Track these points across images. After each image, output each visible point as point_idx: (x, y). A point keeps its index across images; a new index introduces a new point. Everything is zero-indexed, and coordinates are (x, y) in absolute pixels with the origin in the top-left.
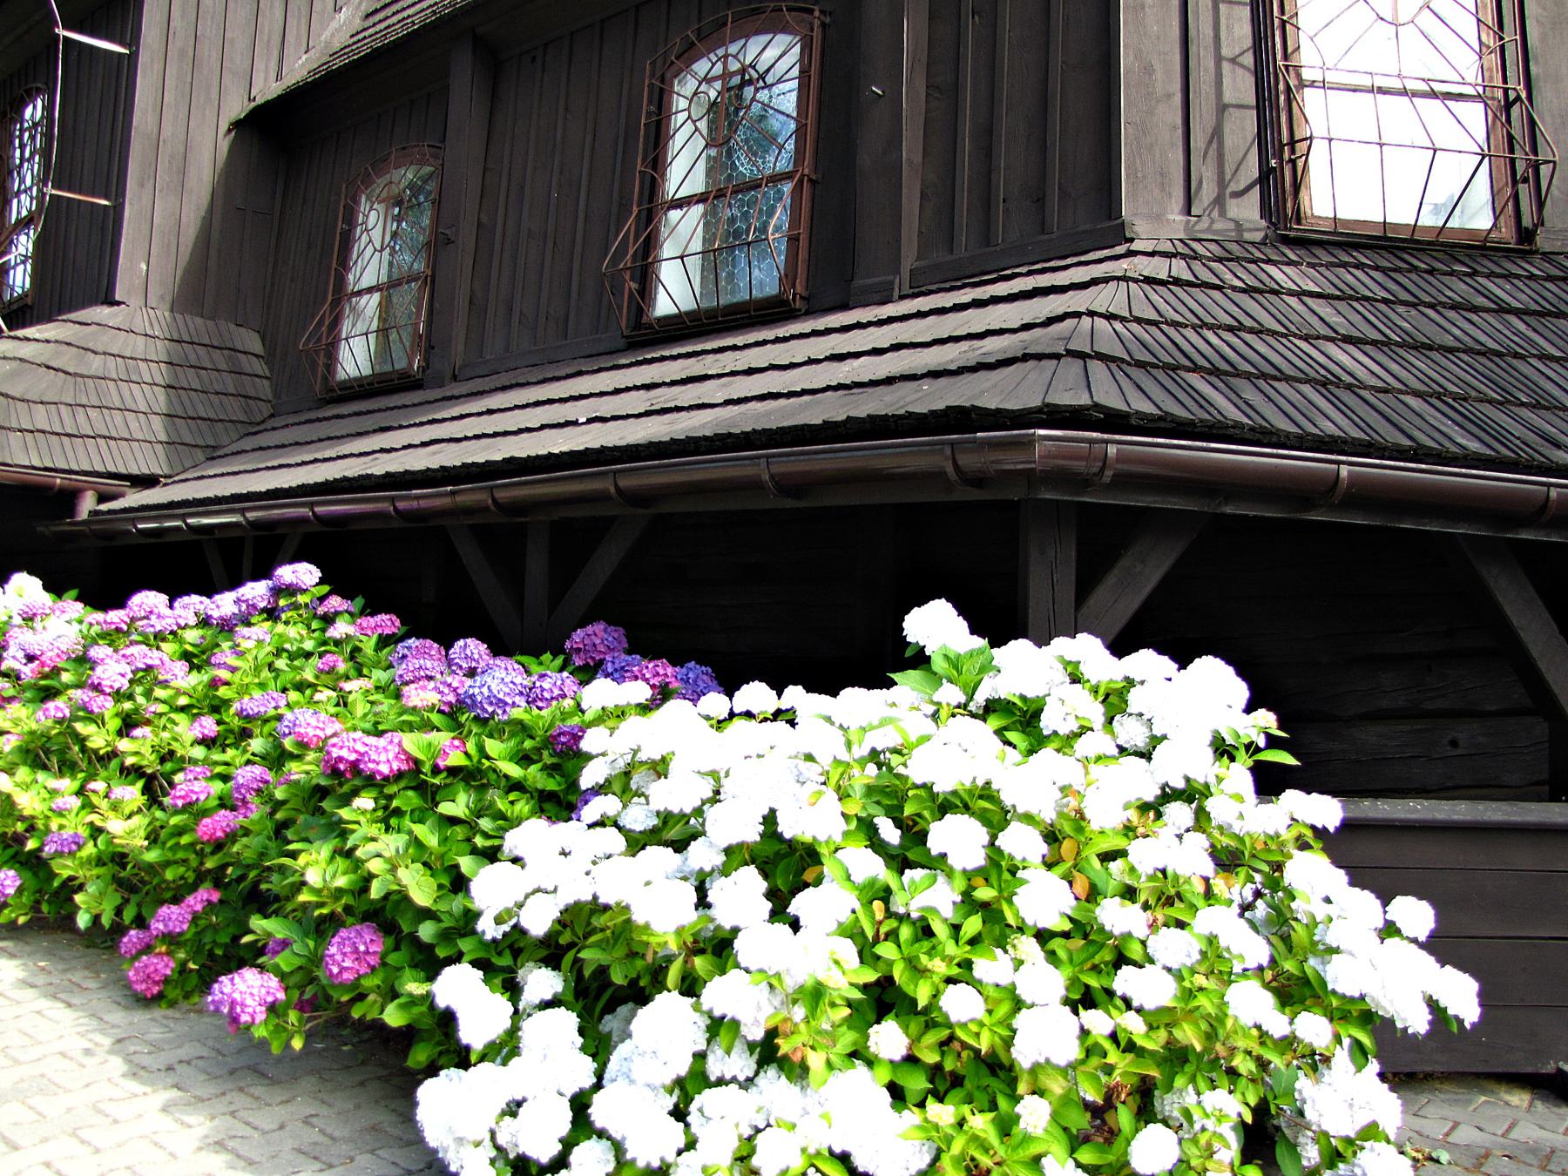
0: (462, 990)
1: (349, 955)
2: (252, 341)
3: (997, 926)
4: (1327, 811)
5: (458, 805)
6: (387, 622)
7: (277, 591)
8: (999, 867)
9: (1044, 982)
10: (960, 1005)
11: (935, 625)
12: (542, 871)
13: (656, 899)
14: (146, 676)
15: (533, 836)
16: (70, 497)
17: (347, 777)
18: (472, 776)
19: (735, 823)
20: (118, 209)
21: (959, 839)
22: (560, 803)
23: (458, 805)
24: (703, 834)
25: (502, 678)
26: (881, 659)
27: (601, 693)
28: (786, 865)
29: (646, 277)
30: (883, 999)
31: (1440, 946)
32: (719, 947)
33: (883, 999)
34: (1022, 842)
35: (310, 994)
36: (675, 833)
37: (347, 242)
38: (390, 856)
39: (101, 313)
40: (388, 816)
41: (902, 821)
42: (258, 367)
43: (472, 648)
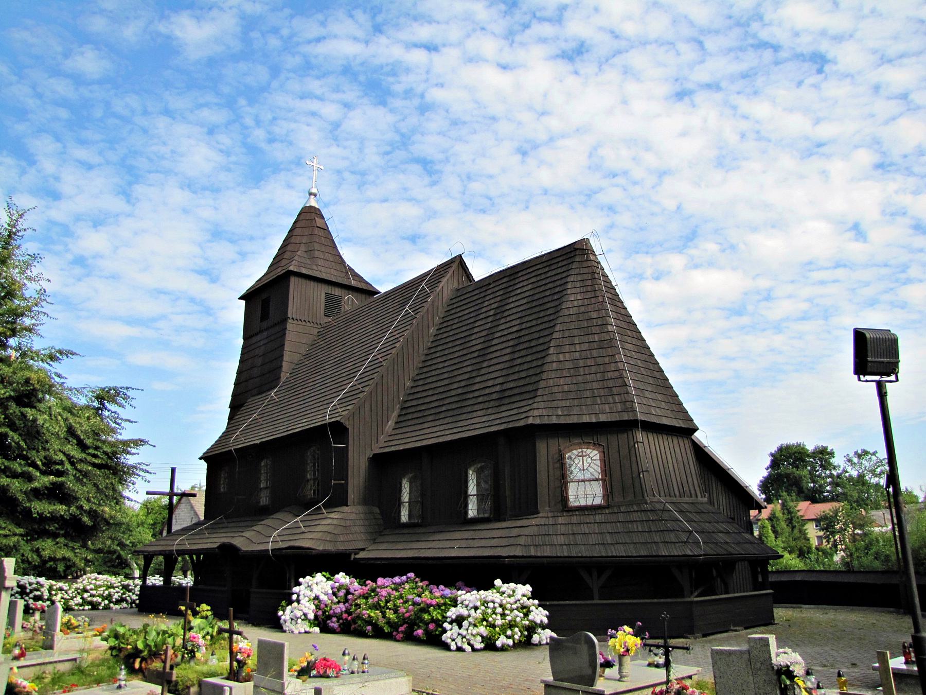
0: (446, 625)
1: (432, 626)
2: (377, 510)
3: (494, 613)
4: (536, 602)
5: (443, 608)
6: (426, 582)
7: (408, 578)
8: (495, 608)
9: (499, 617)
10: (490, 619)
11: (498, 582)
12: (452, 613)
13: (464, 612)
14: (389, 594)
15: (453, 609)
16: (350, 555)
17: (429, 606)
18: (445, 604)
19: (471, 605)
20: (347, 483)
21: (491, 605)
22: (455, 606)
23: (443, 608)
24: (134, 205)
25: (447, 592)
26: (489, 586)
27: (460, 592)
28: (476, 608)
29: (466, 513)
30: (484, 619)
31: (547, 616)
32: (469, 616)
33: (484, 619)
34: (497, 605)
35: (427, 632)
36: (467, 606)
37: (401, 486)
38: (436, 614)
39: (345, 509)
40: (435, 609)
41: (485, 603)
42: (379, 517)
43: (442, 587)
